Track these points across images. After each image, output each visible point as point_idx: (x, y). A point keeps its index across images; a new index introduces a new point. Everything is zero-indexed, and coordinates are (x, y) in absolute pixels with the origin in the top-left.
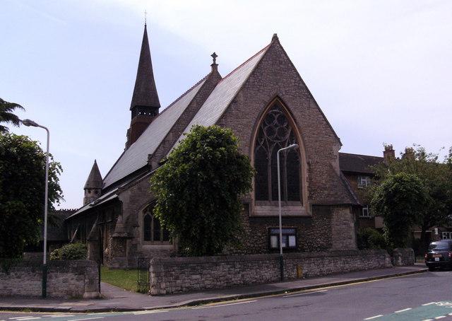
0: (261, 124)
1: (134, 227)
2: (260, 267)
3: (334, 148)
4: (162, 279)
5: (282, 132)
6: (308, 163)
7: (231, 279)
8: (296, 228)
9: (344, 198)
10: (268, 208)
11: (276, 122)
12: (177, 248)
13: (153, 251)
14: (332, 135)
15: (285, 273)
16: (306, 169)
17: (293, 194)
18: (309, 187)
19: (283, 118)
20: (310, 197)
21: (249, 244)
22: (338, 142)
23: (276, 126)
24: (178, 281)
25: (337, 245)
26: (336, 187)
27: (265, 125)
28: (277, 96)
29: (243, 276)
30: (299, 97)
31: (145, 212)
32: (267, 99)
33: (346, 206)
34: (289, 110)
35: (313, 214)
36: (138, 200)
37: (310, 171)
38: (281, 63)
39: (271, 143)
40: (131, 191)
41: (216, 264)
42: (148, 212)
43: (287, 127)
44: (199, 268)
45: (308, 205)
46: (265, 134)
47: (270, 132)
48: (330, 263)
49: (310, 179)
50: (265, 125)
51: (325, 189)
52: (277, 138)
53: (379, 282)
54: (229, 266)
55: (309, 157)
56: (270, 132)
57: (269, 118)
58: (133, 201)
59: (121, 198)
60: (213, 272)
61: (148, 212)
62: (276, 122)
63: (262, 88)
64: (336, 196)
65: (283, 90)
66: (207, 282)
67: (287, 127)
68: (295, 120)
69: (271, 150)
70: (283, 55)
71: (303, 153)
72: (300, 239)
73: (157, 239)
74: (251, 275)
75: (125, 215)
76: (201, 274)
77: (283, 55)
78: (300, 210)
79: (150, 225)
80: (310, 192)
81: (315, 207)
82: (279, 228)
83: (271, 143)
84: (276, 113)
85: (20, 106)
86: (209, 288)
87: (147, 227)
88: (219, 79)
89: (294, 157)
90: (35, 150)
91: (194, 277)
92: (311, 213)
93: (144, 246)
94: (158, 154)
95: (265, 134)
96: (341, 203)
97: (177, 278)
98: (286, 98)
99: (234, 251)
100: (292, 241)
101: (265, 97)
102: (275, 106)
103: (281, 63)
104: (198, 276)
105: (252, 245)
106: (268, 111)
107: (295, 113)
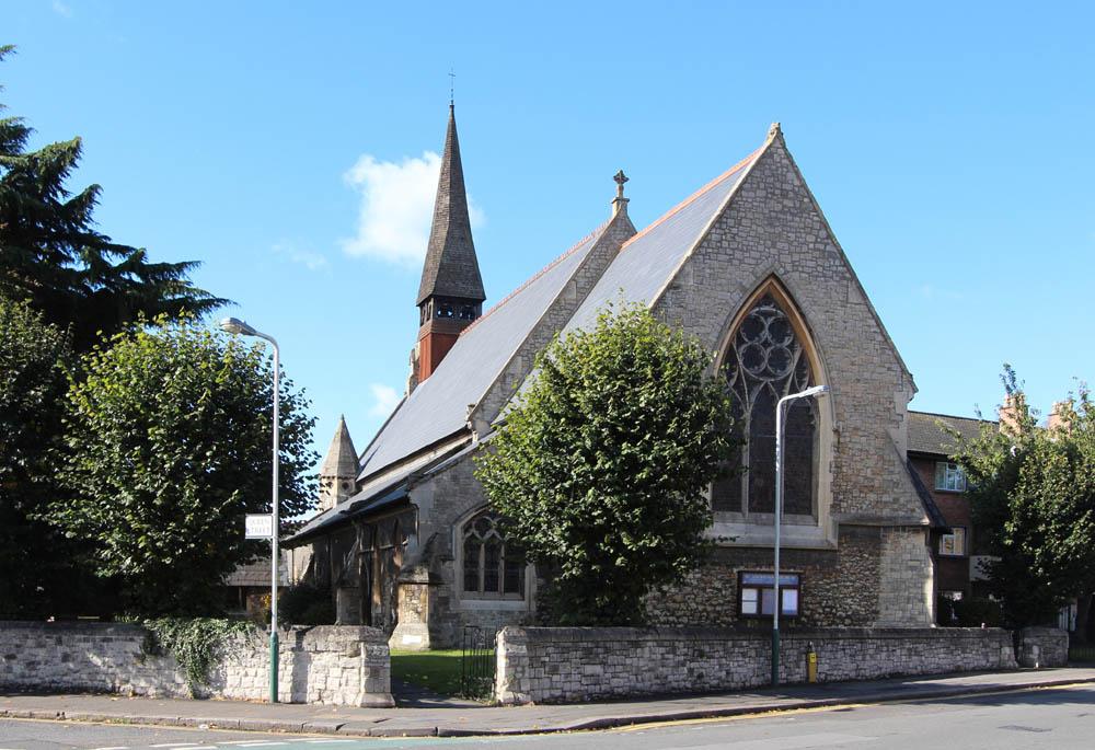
0: (732, 338)
1: (444, 561)
2: (728, 654)
3: (898, 397)
4: (523, 672)
5: (779, 360)
6: (836, 431)
7: (666, 677)
8: (799, 574)
9: (913, 510)
10: (740, 526)
11: (766, 334)
12: (534, 608)
13: (481, 612)
14: (895, 367)
15: (781, 669)
16: (829, 444)
17: (801, 502)
18: (834, 484)
19: (782, 327)
20: (835, 507)
21: (694, 605)
22: (908, 383)
23: (766, 344)
24: (555, 678)
25: (891, 616)
26: (896, 484)
27: (740, 342)
28: (773, 275)
29: (691, 671)
30: (824, 276)
31: (466, 529)
32: (749, 281)
33: (918, 528)
34: (798, 307)
35: (840, 544)
36: (451, 504)
37: (839, 447)
38: (784, 195)
39: (752, 383)
40: (438, 482)
41: (636, 645)
42: (473, 530)
43: (791, 346)
44: (600, 650)
45: (831, 523)
46: (740, 362)
47: (752, 358)
48: (878, 650)
49: (837, 468)
50: (740, 342)
51: (872, 489)
52: (766, 373)
53: (720, 723)
54: (662, 650)
55: (838, 416)
56: (752, 358)
57: (751, 326)
58: (441, 504)
59: (414, 497)
60: (628, 661)
61: (473, 530)
62: (766, 334)
63: (738, 254)
64: (896, 506)
65: (786, 259)
66: (615, 682)
67: (791, 346)
68: (810, 331)
69: (753, 399)
70: (791, 176)
71: (824, 406)
72: (808, 599)
73: (491, 586)
74: (711, 669)
75: (424, 536)
76: (603, 664)
77: (791, 176)
78: (818, 531)
79: (478, 556)
80: (836, 494)
81: (846, 530)
82: (773, 573)
83: (752, 383)
84: (767, 315)
85: (225, 301)
86: (620, 694)
87: (471, 563)
88: (631, 232)
89: (803, 415)
90: (812, 417)
91: (589, 669)
92: (835, 542)
93: (462, 602)
94: (491, 406)
95: (740, 362)
96: (907, 522)
97: (555, 670)
98: (794, 280)
99: (662, 619)
100: (790, 601)
101: (745, 275)
102: (767, 299)
103: (784, 195)
104: (598, 669)
105: (700, 608)
106: (752, 307)
107: (811, 316)
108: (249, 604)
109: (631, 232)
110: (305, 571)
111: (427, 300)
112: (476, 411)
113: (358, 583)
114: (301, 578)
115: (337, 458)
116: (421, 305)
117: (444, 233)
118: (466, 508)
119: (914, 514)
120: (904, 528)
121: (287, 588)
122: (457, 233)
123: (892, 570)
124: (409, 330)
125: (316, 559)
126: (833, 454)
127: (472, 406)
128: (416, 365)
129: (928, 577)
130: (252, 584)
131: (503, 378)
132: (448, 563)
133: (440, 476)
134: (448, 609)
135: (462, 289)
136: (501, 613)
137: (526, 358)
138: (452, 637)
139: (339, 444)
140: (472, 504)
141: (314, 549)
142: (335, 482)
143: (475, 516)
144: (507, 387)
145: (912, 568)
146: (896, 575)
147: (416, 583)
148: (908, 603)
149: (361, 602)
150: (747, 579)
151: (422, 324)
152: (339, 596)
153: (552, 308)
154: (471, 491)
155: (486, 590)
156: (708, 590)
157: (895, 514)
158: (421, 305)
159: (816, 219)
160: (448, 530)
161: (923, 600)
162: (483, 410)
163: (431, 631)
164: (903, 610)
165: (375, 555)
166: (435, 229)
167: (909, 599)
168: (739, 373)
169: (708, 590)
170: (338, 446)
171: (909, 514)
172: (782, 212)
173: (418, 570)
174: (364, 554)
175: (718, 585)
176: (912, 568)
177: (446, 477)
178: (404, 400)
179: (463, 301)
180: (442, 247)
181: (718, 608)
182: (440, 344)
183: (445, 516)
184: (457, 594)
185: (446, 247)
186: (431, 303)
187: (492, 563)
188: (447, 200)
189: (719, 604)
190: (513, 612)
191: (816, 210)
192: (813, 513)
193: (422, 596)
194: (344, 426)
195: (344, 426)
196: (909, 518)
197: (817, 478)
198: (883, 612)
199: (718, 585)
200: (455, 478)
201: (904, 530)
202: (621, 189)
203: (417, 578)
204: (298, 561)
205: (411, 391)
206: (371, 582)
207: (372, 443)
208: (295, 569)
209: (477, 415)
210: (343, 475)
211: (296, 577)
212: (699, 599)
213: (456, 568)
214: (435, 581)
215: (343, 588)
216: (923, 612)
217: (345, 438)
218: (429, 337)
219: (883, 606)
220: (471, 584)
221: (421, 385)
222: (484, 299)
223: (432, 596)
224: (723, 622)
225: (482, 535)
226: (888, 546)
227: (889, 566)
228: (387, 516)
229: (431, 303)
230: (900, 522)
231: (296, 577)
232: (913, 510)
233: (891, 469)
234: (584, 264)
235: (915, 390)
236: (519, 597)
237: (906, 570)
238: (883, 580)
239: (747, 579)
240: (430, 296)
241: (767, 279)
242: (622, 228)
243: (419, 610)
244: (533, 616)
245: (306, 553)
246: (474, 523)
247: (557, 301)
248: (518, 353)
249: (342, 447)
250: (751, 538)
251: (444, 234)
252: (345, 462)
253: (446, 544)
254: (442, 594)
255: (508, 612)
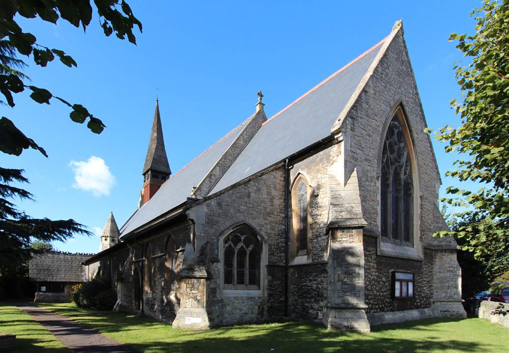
1: (213, 262)
9: (450, 242)
12: (266, 295)
19: (401, 135)
34: (409, 126)
36: (218, 222)
45: (421, 246)
59: (192, 214)
73: (241, 281)
75: (198, 244)
78: (415, 251)
87: (228, 263)
92: (422, 256)
94: (205, 189)
107: (415, 135)
108: (66, 290)
109: (265, 119)
110: (95, 274)
111: (148, 171)
112: (197, 190)
113: (131, 279)
114: (94, 277)
115: (109, 229)
116: (144, 174)
117: (154, 146)
118: (226, 226)
119: (451, 244)
120: (445, 251)
121: (85, 283)
122: (160, 147)
123: (439, 272)
124: (140, 184)
125: (102, 268)
126: (420, 210)
127: (194, 188)
128: (142, 196)
129: (458, 276)
130: (68, 281)
131: (210, 176)
132: (215, 264)
133: (210, 201)
134: (216, 297)
135: (162, 168)
136: (248, 298)
137: (221, 168)
138: (218, 316)
139: (110, 223)
140: (230, 225)
141: (100, 264)
142: (109, 239)
143: (232, 233)
144: (212, 181)
145: (450, 271)
146: (442, 275)
147: (197, 278)
148: (448, 289)
149: (133, 291)
150: (399, 276)
151: (145, 182)
152: (119, 287)
153: (233, 146)
154: (229, 215)
155: (250, 283)
156: (381, 283)
157: (441, 244)
158: (144, 174)
159: (413, 82)
160: (215, 241)
161: (456, 287)
162: (201, 190)
163: (209, 313)
164: (446, 293)
165: (146, 262)
166: (150, 147)
167: (449, 287)
168: (387, 157)
169: (381, 283)
170: (110, 224)
171: (448, 244)
172: (402, 71)
173: (197, 269)
174: (134, 262)
175: (384, 279)
176: (450, 271)
177: (213, 202)
178: (137, 211)
179: (162, 173)
180: (154, 151)
181: (384, 294)
182: (153, 189)
183: (213, 230)
184: (221, 287)
185: (155, 152)
186: (150, 172)
187: (241, 265)
188: (156, 135)
189: (385, 291)
190: (255, 298)
191: (413, 77)
192: (411, 241)
193: (201, 288)
194: (112, 216)
195: (112, 216)
196: (449, 246)
197: (413, 222)
198: (435, 294)
199: (384, 279)
200: (219, 204)
201: (445, 252)
202: (261, 99)
203: (197, 274)
204: (91, 271)
205: (140, 207)
206: (143, 279)
207: (125, 224)
208: (90, 274)
209: (198, 192)
210: (112, 235)
211: (90, 276)
212: (377, 288)
213: (220, 267)
214: (209, 278)
215: (122, 282)
216: (456, 293)
217: (113, 221)
218: (149, 186)
219: (435, 291)
220: (228, 280)
221: (145, 205)
222: (171, 174)
223: (208, 286)
224: (386, 302)
225: (235, 245)
226: (437, 260)
227: (438, 270)
228: (150, 239)
229: (150, 172)
230: (445, 248)
231: (90, 276)
232: (450, 242)
233: (438, 220)
234: (246, 129)
235: (441, 184)
236: (257, 288)
237: (447, 272)
238: (435, 277)
239: (399, 276)
240: (149, 169)
241: (398, 106)
242: (261, 117)
243: (199, 298)
244: (266, 300)
245: (95, 266)
246: (231, 238)
247: (235, 143)
248: (217, 165)
249: (112, 225)
250: (396, 252)
251: (155, 147)
252: (113, 231)
253: (214, 250)
254: (212, 286)
255: (252, 298)
